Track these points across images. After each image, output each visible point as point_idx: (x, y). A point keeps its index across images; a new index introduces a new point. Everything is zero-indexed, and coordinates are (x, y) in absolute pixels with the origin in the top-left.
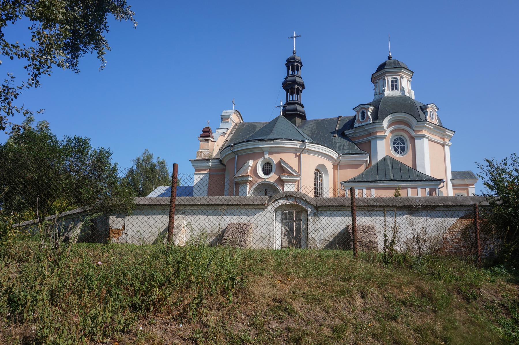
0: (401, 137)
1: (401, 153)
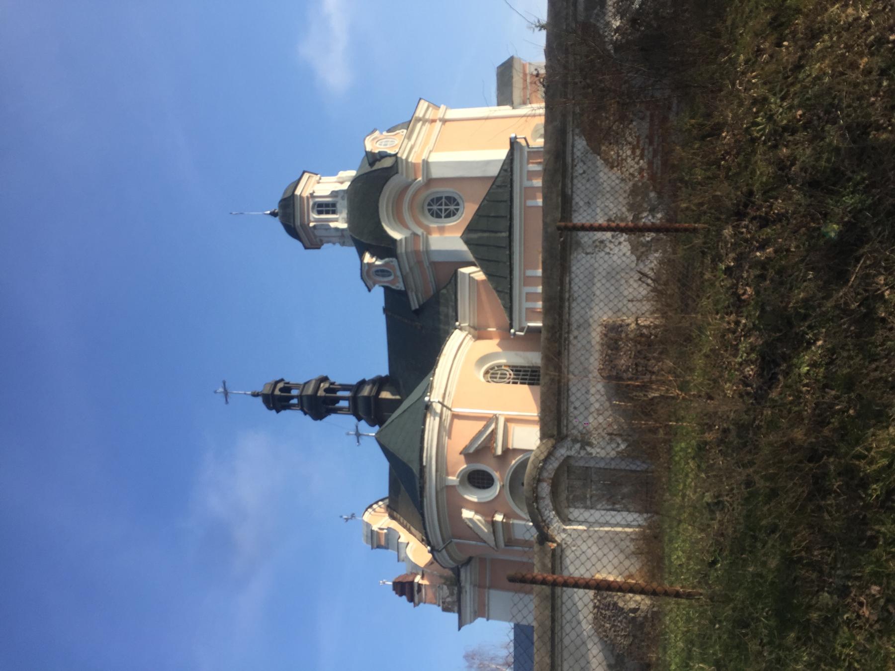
0: (427, 203)
1: (458, 204)
